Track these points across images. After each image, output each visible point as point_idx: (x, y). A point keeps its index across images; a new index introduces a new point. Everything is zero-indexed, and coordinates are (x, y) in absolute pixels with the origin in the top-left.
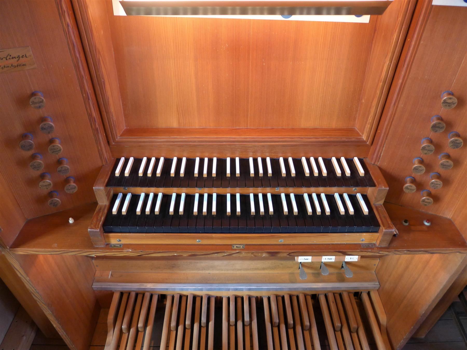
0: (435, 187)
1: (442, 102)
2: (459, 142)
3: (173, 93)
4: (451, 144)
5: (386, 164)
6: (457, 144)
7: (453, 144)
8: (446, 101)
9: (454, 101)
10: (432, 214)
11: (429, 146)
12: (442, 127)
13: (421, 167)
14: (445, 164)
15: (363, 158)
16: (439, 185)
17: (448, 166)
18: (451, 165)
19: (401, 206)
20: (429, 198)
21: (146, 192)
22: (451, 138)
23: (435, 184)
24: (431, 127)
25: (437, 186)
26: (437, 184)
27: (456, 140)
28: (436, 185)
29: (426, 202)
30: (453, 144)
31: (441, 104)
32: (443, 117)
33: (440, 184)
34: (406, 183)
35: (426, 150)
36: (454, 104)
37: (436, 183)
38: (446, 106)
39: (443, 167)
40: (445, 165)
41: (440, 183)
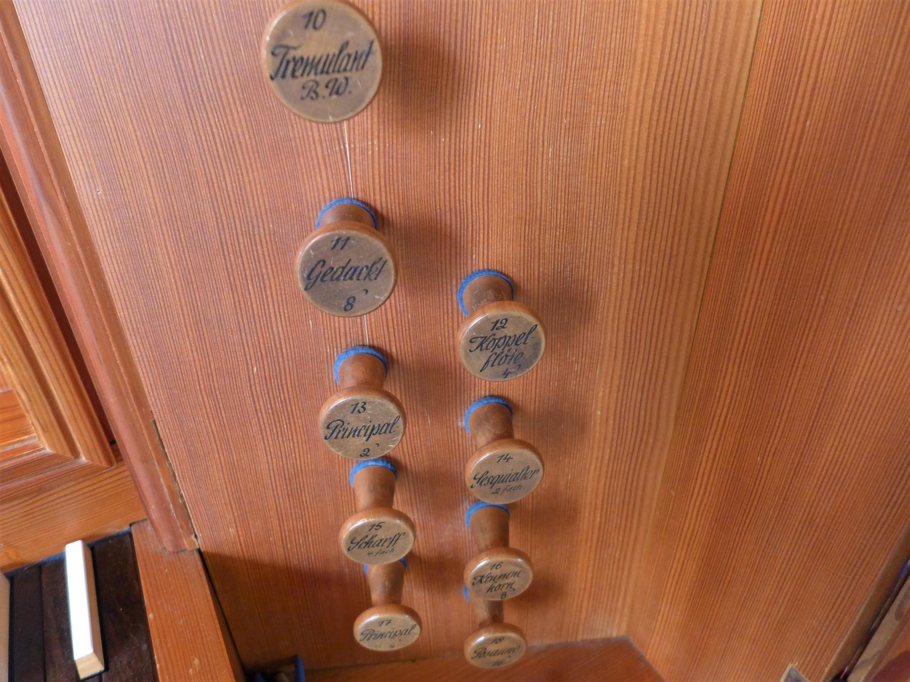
0: (504, 589)
1: (267, 73)
2: (518, 333)
3: (894, 247)
4: (482, 358)
5: (232, 530)
6: (513, 347)
7: (489, 353)
8: (292, 54)
9: (349, 35)
10: (550, 647)
11: (357, 408)
12: (370, 269)
13: (379, 526)
14: (496, 471)
15: (126, 528)
16: (516, 574)
17: (515, 477)
18: (532, 468)
19: (413, 661)
20: (499, 635)
21: (84, 534)
22: (472, 315)
23: (493, 579)
24: (301, 286)
25: (510, 585)
26: (505, 576)
27: (498, 324)
28: (501, 582)
29: (497, 653)
30: (489, 353)
31: (273, 84)
32: (379, 201)
33: (517, 569)
34: (366, 604)
35: (355, 432)
36: (359, 60)
37: (496, 572)
38: (313, 94)
39: (494, 490)
40: (500, 479)
41: (517, 565)
